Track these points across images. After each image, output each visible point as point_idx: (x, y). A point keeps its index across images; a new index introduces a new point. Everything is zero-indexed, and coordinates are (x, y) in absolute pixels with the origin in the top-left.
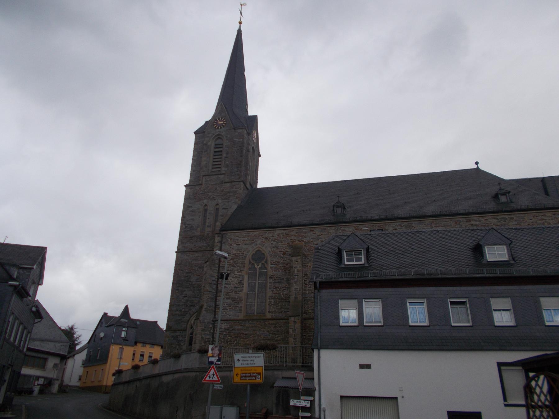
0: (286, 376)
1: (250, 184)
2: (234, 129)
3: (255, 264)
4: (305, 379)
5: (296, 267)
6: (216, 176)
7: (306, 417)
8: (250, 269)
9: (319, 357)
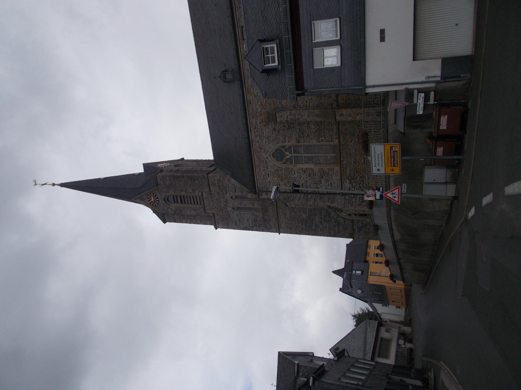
0: (394, 118)
1: (210, 167)
2: (157, 185)
3: (287, 157)
4: (396, 100)
5: (287, 117)
6: (205, 200)
7: (435, 96)
8: (291, 163)
9: (374, 86)
